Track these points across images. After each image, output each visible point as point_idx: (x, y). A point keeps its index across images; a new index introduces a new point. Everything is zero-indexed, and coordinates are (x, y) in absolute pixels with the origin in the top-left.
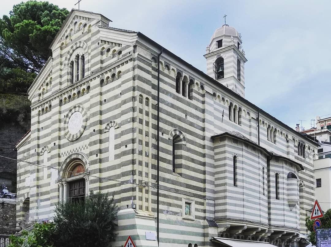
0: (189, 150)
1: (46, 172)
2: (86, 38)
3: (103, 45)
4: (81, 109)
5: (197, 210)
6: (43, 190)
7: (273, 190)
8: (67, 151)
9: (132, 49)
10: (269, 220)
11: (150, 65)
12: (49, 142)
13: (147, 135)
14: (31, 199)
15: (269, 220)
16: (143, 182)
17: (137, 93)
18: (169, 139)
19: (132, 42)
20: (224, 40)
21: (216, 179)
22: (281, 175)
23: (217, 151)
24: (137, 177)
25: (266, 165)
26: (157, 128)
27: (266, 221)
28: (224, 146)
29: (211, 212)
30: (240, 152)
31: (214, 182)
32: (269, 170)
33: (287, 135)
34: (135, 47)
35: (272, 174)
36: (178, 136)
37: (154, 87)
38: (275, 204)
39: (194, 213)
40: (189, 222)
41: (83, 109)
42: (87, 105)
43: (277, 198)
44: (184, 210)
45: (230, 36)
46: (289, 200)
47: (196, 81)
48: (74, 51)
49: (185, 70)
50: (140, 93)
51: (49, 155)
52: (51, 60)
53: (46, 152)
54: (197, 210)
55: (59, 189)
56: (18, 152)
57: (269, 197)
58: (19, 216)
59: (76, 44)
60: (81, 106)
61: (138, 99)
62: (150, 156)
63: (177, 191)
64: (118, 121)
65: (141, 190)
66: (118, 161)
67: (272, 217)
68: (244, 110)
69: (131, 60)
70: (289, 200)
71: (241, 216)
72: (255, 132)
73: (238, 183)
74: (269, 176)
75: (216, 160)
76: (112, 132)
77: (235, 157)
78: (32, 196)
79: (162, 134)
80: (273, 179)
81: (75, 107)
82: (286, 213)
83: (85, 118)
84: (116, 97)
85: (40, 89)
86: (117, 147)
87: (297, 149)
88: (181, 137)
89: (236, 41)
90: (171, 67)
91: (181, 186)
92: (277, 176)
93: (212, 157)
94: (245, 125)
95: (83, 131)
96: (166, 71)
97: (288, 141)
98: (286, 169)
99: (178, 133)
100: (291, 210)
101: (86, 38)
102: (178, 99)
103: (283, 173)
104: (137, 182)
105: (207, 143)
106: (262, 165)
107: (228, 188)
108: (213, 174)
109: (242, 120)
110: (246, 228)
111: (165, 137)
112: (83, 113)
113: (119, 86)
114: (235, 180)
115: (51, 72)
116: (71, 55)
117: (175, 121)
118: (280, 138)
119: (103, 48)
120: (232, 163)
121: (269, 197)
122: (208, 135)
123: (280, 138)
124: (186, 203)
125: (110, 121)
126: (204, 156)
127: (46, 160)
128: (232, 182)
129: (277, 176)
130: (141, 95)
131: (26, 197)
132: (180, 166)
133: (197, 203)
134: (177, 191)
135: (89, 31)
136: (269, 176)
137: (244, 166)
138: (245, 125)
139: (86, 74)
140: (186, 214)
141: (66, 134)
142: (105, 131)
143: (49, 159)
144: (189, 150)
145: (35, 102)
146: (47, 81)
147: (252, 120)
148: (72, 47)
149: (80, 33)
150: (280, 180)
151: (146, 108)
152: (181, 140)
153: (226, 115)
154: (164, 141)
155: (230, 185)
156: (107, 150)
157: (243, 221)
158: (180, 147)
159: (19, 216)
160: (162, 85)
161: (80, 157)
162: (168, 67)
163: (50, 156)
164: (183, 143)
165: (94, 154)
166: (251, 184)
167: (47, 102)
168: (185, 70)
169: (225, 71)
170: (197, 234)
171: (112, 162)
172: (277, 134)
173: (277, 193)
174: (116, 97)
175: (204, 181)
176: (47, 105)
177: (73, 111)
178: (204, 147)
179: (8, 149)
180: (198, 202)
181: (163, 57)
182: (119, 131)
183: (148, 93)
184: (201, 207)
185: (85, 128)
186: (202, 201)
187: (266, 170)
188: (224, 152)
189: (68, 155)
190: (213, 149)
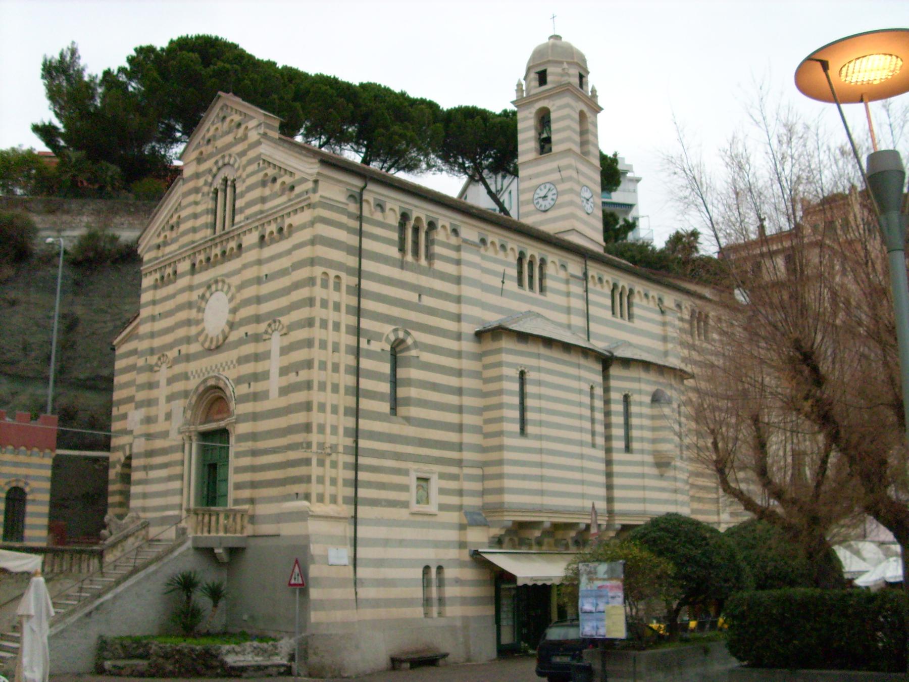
0: (428, 367)
1: (162, 409)
2: (239, 148)
3: (265, 168)
4: (226, 288)
5: (442, 491)
6: (159, 444)
7: (618, 432)
8: (201, 370)
9: (310, 185)
10: (610, 500)
11: (344, 211)
12: (171, 346)
13: (336, 349)
14: (135, 463)
15: (610, 500)
16: (327, 445)
17: (318, 271)
18: (383, 350)
19: (312, 175)
20: (550, 70)
21: (487, 421)
22: (635, 398)
23: (489, 360)
24: (315, 438)
25: (599, 379)
26: (358, 332)
27: (602, 505)
28: (499, 351)
29: (473, 493)
30: (533, 362)
31: (481, 427)
32: (607, 390)
33: (660, 299)
34: (316, 182)
35: (615, 396)
36: (401, 342)
37: (349, 250)
38: (621, 463)
39: (436, 499)
40: (426, 519)
41: (229, 287)
42: (235, 281)
43: (628, 449)
44: (412, 496)
45: (562, 63)
46: (655, 453)
47: (440, 224)
48: (219, 169)
49: (416, 206)
50: (323, 269)
51: (170, 373)
52: (181, 182)
53: (164, 366)
54: (442, 491)
55: (184, 445)
56: (118, 352)
57: (608, 450)
58: (114, 493)
59: (223, 157)
60: (227, 280)
61: (319, 281)
62: (342, 390)
63: (398, 456)
64: (285, 320)
65: (321, 463)
66: (283, 402)
67: (617, 493)
68: (553, 262)
69: (309, 206)
70: (655, 453)
71: (536, 500)
72: (578, 304)
73: (530, 429)
74: (607, 402)
75: (486, 381)
76: (276, 343)
77: (522, 373)
78: (139, 455)
79: (369, 342)
80: (617, 408)
81: (216, 282)
82: (648, 482)
83: (233, 305)
84: (284, 272)
85: (159, 235)
86: (284, 371)
87: (687, 326)
88: (409, 341)
89: (574, 71)
90: (388, 206)
91: (408, 444)
92: (626, 399)
93: (477, 375)
94: (556, 292)
95: (229, 333)
96: (378, 216)
97: (663, 312)
98: (648, 382)
99: (401, 335)
100: (662, 476)
101: (239, 148)
102: (403, 265)
103: (640, 392)
104: (314, 447)
105: (468, 346)
106: (586, 380)
107: (507, 441)
108: (479, 411)
109: (549, 283)
110: (547, 525)
111: (375, 346)
112: (230, 295)
113: (289, 252)
114: (523, 422)
115: (180, 204)
116: (214, 176)
117: (396, 312)
118: (645, 308)
119: (266, 175)
120: (516, 387)
121: (608, 450)
122: (469, 329)
123: (645, 308)
124: (418, 479)
125: (273, 317)
126: (459, 373)
127: (163, 382)
128: (516, 427)
129: (626, 399)
130: (325, 273)
131: (128, 453)
132: (408, 402)
133: (442, 476)
134: (398, 456)
135: (245, 138)
136: (607, 402)
137: (544, 391)
138: (556, 292)
139: (238, 218)
140: (418, 502)
141: (199, 334)
142: (267, 337)
143: (170, 381)
144: (428, 367)
145: (150, 261)
146: (171, 222)
147: (572, 280)
148: (216, 163)
149: (229, 138)
150: (634, 409)
151: (334, 296)
152: (408, 348)
153: (511, 278)
154: (371, 355)
155: (511, 435)
156: (265, 376)
157: (540, 511)
158: (408, 363)
159: (114, 493)
160: (367, 244)
161: (221, 385)
162: (380, 206)
163: (170, 375)
164: (413, 353)
165: (244, 382)
166: (559, 426)
167: (170, 264)
168: (416, 206)
169: (554, 138)
170: (446, 545)
171: (275, 401)
172: (636, 300)
173: (628, 439)
174: (284, 272)
175: (460, 428)
176: (169, 270)
177: (214, 288)
178: (459, 355)
179: (105, 322)
180: (445, 474)
181: (371, 191)
182: (286, 341)
183: (340, 266)
184: (452, 485)
185: (232, 325)
186: (454, 470)
187: (599, 391)
188: (499, 364)
189: (202, 378)
190: (479, 357)
